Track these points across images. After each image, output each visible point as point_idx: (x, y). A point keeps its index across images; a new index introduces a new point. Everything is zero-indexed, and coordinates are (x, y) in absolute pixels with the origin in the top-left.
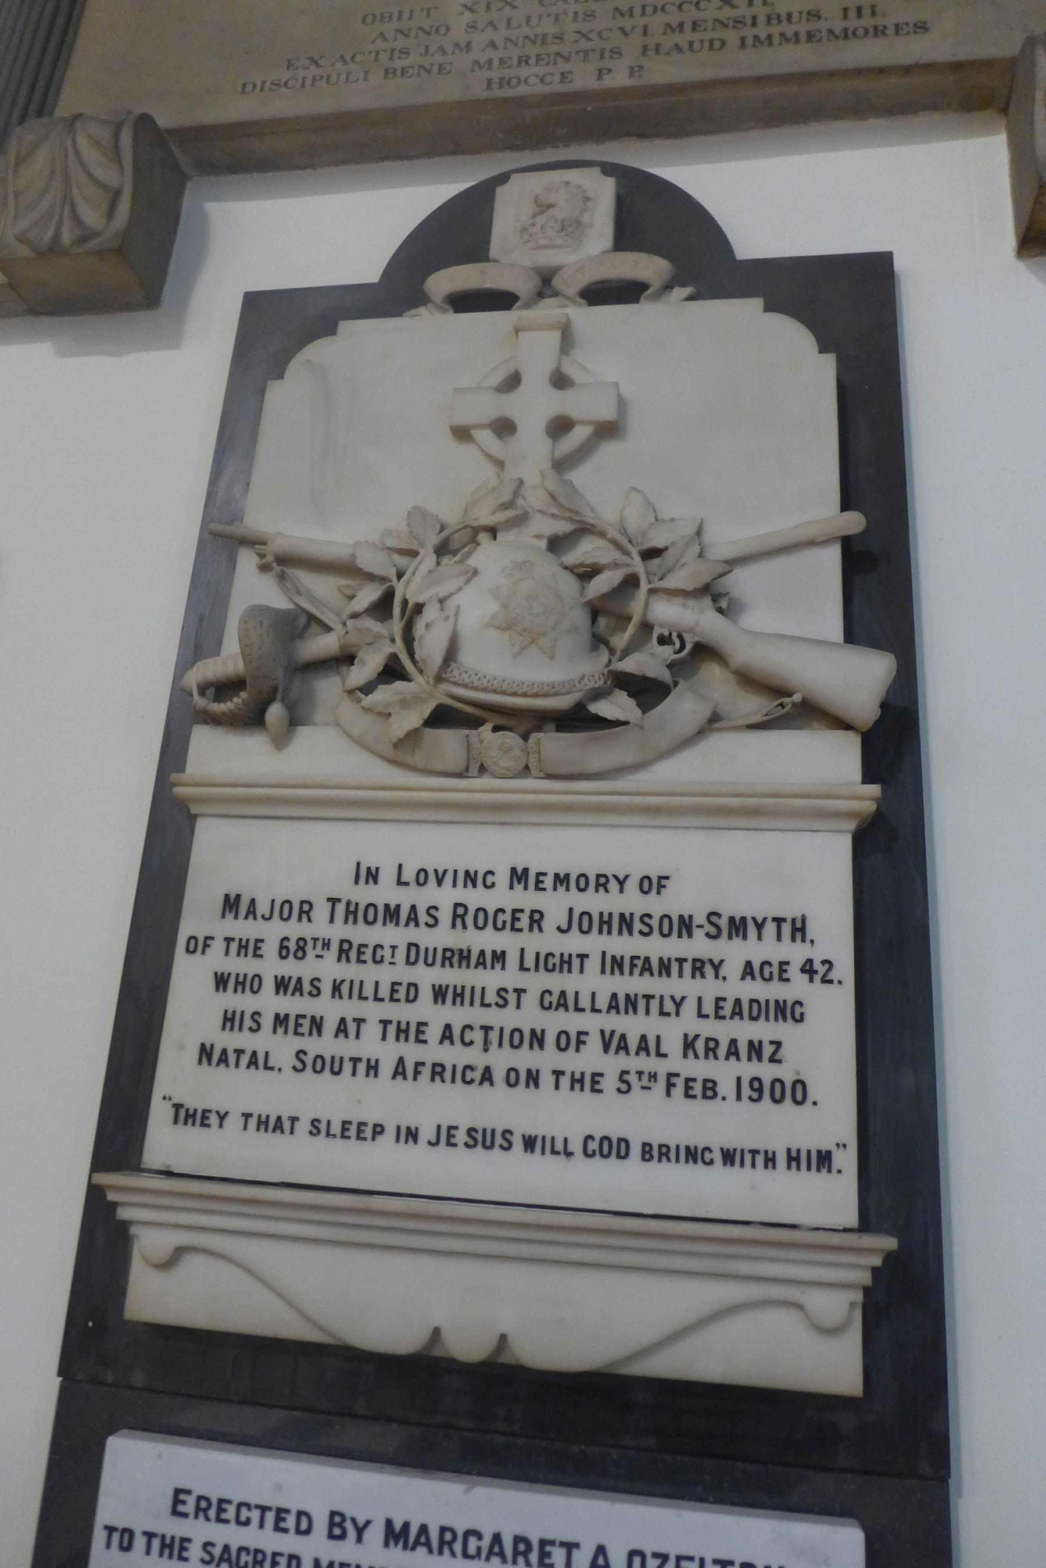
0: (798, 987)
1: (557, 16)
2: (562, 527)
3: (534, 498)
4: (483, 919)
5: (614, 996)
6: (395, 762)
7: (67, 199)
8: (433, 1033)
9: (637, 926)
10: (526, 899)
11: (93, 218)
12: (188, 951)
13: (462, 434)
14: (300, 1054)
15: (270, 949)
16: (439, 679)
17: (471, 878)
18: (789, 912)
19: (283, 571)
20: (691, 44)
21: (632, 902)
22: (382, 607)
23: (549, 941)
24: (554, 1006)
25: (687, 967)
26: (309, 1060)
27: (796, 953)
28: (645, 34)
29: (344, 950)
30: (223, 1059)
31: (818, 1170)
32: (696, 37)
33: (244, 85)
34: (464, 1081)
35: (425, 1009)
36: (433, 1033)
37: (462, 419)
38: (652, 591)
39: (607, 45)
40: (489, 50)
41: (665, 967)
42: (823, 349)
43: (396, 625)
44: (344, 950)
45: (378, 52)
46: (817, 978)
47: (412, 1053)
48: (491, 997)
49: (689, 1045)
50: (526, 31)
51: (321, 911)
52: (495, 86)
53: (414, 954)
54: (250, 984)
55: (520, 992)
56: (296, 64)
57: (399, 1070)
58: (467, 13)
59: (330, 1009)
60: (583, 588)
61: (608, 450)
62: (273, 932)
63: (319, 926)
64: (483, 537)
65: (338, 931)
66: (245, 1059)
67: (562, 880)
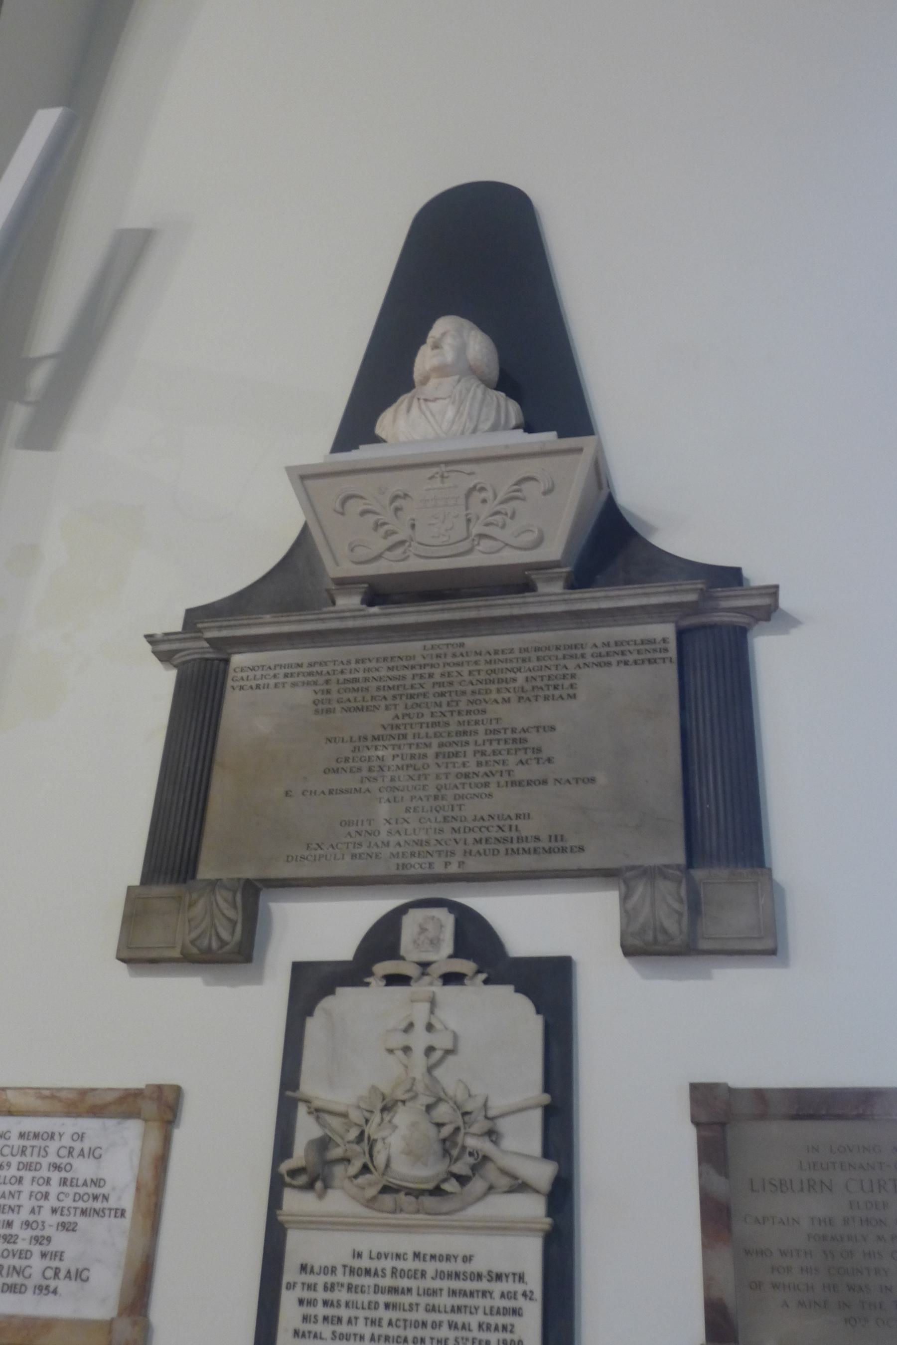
0: (521, 1302)
1: (427, 829)
2: (430, 1100)
3: (420, 1087)
4: (403, 1274)
5: (453, 1307)
6: (367, 1207)
7: (213, 925)
8: (385, 1323)
9: (462, 1276)
10: (419, 1265)
11: (225, 935)
12: (287, 1288)
13: (391, 1051)
14: (334, 1333)
15: (320, 1287)
16: (383, 1174)
17: (398, 1256)
18: (518, 1270)
19: (318, 1115)
20: (485, 851)
21: (460, 1266)
22: (360, 1138)
23: (429, 1283)
24: (431, 1310)
25: (480, 1294)
26: (337, 1335)
27: (519, 1288)
28: (465, 843)
29: (350, 1288)
30: (304, 1335)
31: (452, 1296)
32: (488, 847)
33: (288, 857)
34: (397, 1342)
35: (381, 1313)
36: (385, 1323)
37: (390, 1046)
38: (466, 1134)
39: (449, 849)
40: (398, 847)
41: (472, 1294)
42: (538, 1012)
43: (366, 1147)
44: (350, 1288)
45: (348, 843)
46: (528, 1298)
47: (377, 1331)
48: (407, 1307)
49: (480, 1326)
50: (414, 837)
51: (340, 1270)
52: (400, 868)
53: (377, 1289)
54: (312, 1303)
55: (417, 1305)
56: (311, 846)
57: (372, 1339)
58: (387, 824)
59: (345, 1313)
60: (439, 1132)
61: (451, 1059)
62: (321, 1280)
63: (341, 1277)
64: (400, 1104)
65: (347, 1279)
66: (312, 1336)
67: (433, 1257)
